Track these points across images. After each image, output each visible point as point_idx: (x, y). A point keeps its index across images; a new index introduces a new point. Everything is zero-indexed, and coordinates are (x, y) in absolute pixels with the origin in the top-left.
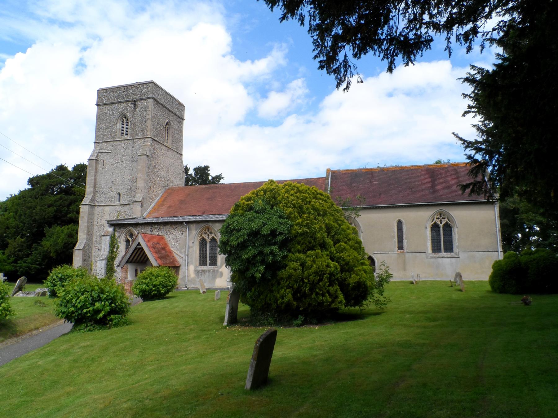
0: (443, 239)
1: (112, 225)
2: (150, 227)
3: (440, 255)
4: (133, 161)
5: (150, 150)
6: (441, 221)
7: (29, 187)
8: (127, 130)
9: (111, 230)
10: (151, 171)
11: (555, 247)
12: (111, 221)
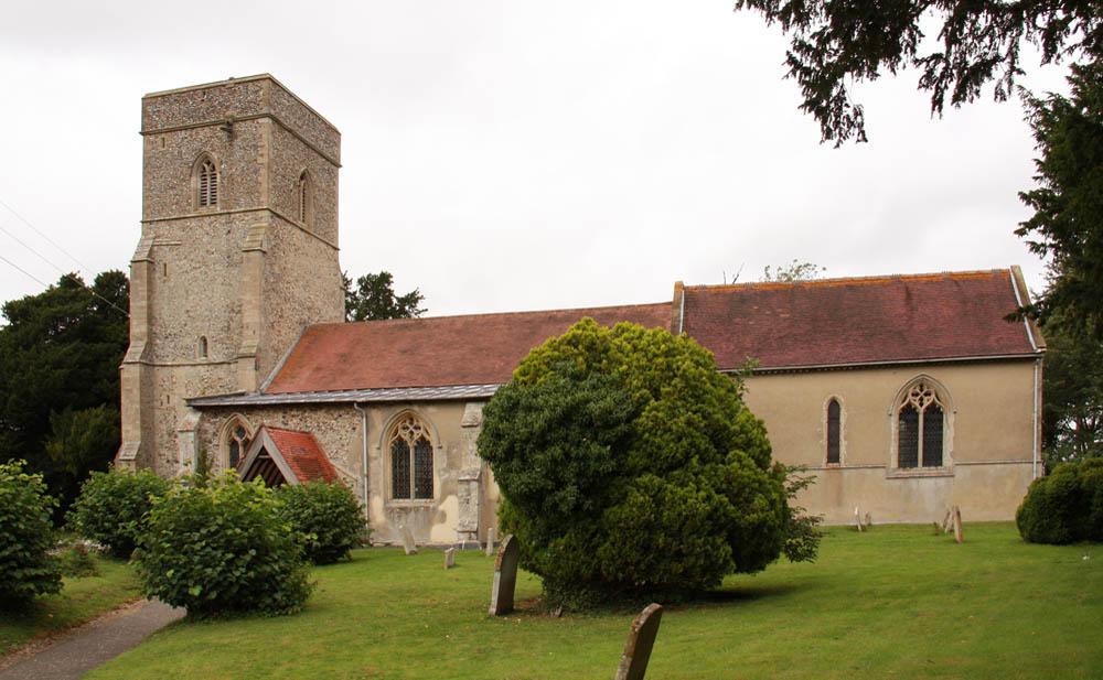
0: (921, 436)
1: (198, 409)
2: (280, 415)
3: (913, 471)
4: (229, 265)
5: (269, 240)
6: (921, 399)
7: (7, 323)
8: (213, 192)
9: (194, 418)
10: (272, 287)
11: (1099, 443)
12: (195, 400)
